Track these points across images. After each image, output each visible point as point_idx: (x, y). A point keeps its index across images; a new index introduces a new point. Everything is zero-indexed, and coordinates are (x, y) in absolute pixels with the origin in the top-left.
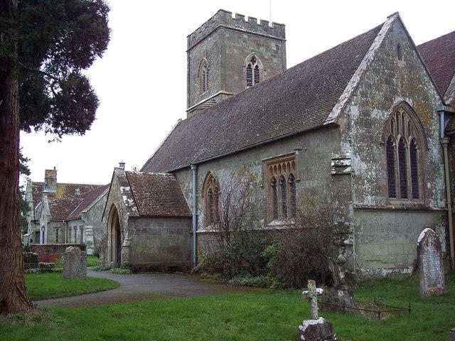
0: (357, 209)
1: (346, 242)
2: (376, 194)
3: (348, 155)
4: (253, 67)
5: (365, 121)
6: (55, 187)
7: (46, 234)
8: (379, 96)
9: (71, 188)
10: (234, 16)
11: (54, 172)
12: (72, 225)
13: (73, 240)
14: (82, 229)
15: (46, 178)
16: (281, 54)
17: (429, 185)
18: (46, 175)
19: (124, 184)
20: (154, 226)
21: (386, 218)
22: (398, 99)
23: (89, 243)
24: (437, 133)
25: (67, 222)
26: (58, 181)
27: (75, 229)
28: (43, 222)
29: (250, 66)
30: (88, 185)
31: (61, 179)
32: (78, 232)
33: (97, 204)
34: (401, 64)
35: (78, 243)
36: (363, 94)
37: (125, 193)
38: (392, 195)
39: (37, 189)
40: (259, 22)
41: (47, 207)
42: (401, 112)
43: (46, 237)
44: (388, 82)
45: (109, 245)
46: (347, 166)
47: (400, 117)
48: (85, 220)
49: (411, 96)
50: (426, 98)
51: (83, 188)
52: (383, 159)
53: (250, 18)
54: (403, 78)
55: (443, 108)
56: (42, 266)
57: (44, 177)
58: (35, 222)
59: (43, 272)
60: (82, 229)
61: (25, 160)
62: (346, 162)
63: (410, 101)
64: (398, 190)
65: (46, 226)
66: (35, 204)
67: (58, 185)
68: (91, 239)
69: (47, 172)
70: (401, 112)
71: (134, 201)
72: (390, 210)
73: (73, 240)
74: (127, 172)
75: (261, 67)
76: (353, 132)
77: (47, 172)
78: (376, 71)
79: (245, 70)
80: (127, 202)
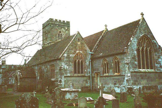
0: (65, 77)
1: (61, 84)
2: (71, 73)
3: (63, 65)
4: (60, 34)
5: (68, 57)
8: (73, 51)
9: (10, 66)
10: (54, 20)
11: (5, 61)
16: (68, 30)
17: (85, 71)
20: (26, 80)
21: (73, 78)
22: (78, 52)
24: (88, 59)
29: (59, 34)
34: (79, 43)
36: (68, 51)
37: (19, 72)
38: (75, 73)
40: (62, 21)
42: (79, 54)
44: (75, 48)
46: (62, 68)
47: (78, 56)
49: (81, 50)
50: (86, 50)
52: (73, 65)
53: (59, 20)
54: (79, 47)
55: (90, 53)
62: (62, 67)
63: (81, 52)
64: (77, 72)
70: (79, 54)
71: (22, 74)
72: (74, 77)
75: (62, 34)
76: (65, 60)
78: (72, 46)
79: (57, 35)
80: (19, 74)
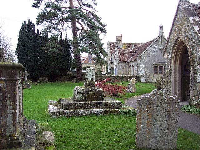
6: (122, 45)
7: (117, 69)
9: (130, 45)
11: (121, 37)
12: (131, 64)
13: (132, 73)
14: (137, 67)
15: (117, 40)
18: (117, 39)
19: (194, 15)
23: (142, 75)
25: (128, 63)
26: (123, 42)
27: (133, 66)
28: (116, 63)
30: (138, 44)
31: (125, 40)
32: (135, 68)
33: (147, 51)
35: (135, 75)
39: (112, 46)
41: (117, 54)
43: (117, 71)
45: (172, 78)
48: (140, 61)
51: (136, 45)
56: (108, 105)
57: (116, 40)
58: (112, 63)
59: (107, 113)
60: (137, 67)
61: (104, 26)
65: (117, 65)
66: (111, 54)
67: (123, 44)
68: (143, 72)
69: (117, 37)
73: (132, 73)
74: (193, 5)
77: (117, 37)
